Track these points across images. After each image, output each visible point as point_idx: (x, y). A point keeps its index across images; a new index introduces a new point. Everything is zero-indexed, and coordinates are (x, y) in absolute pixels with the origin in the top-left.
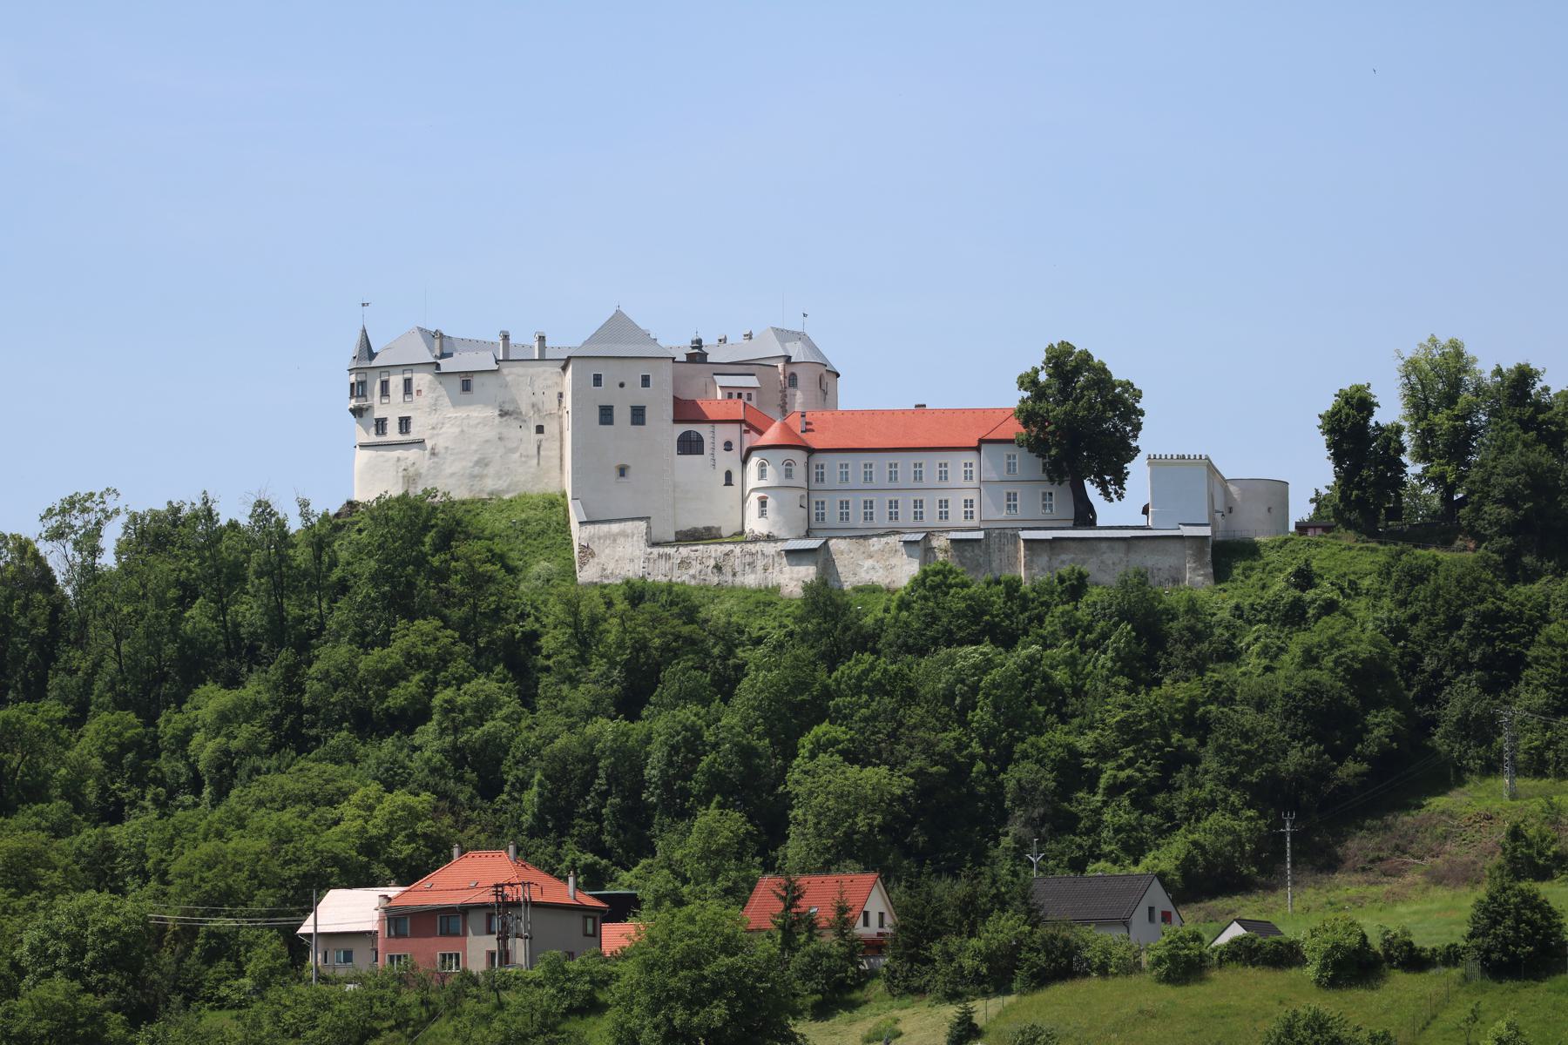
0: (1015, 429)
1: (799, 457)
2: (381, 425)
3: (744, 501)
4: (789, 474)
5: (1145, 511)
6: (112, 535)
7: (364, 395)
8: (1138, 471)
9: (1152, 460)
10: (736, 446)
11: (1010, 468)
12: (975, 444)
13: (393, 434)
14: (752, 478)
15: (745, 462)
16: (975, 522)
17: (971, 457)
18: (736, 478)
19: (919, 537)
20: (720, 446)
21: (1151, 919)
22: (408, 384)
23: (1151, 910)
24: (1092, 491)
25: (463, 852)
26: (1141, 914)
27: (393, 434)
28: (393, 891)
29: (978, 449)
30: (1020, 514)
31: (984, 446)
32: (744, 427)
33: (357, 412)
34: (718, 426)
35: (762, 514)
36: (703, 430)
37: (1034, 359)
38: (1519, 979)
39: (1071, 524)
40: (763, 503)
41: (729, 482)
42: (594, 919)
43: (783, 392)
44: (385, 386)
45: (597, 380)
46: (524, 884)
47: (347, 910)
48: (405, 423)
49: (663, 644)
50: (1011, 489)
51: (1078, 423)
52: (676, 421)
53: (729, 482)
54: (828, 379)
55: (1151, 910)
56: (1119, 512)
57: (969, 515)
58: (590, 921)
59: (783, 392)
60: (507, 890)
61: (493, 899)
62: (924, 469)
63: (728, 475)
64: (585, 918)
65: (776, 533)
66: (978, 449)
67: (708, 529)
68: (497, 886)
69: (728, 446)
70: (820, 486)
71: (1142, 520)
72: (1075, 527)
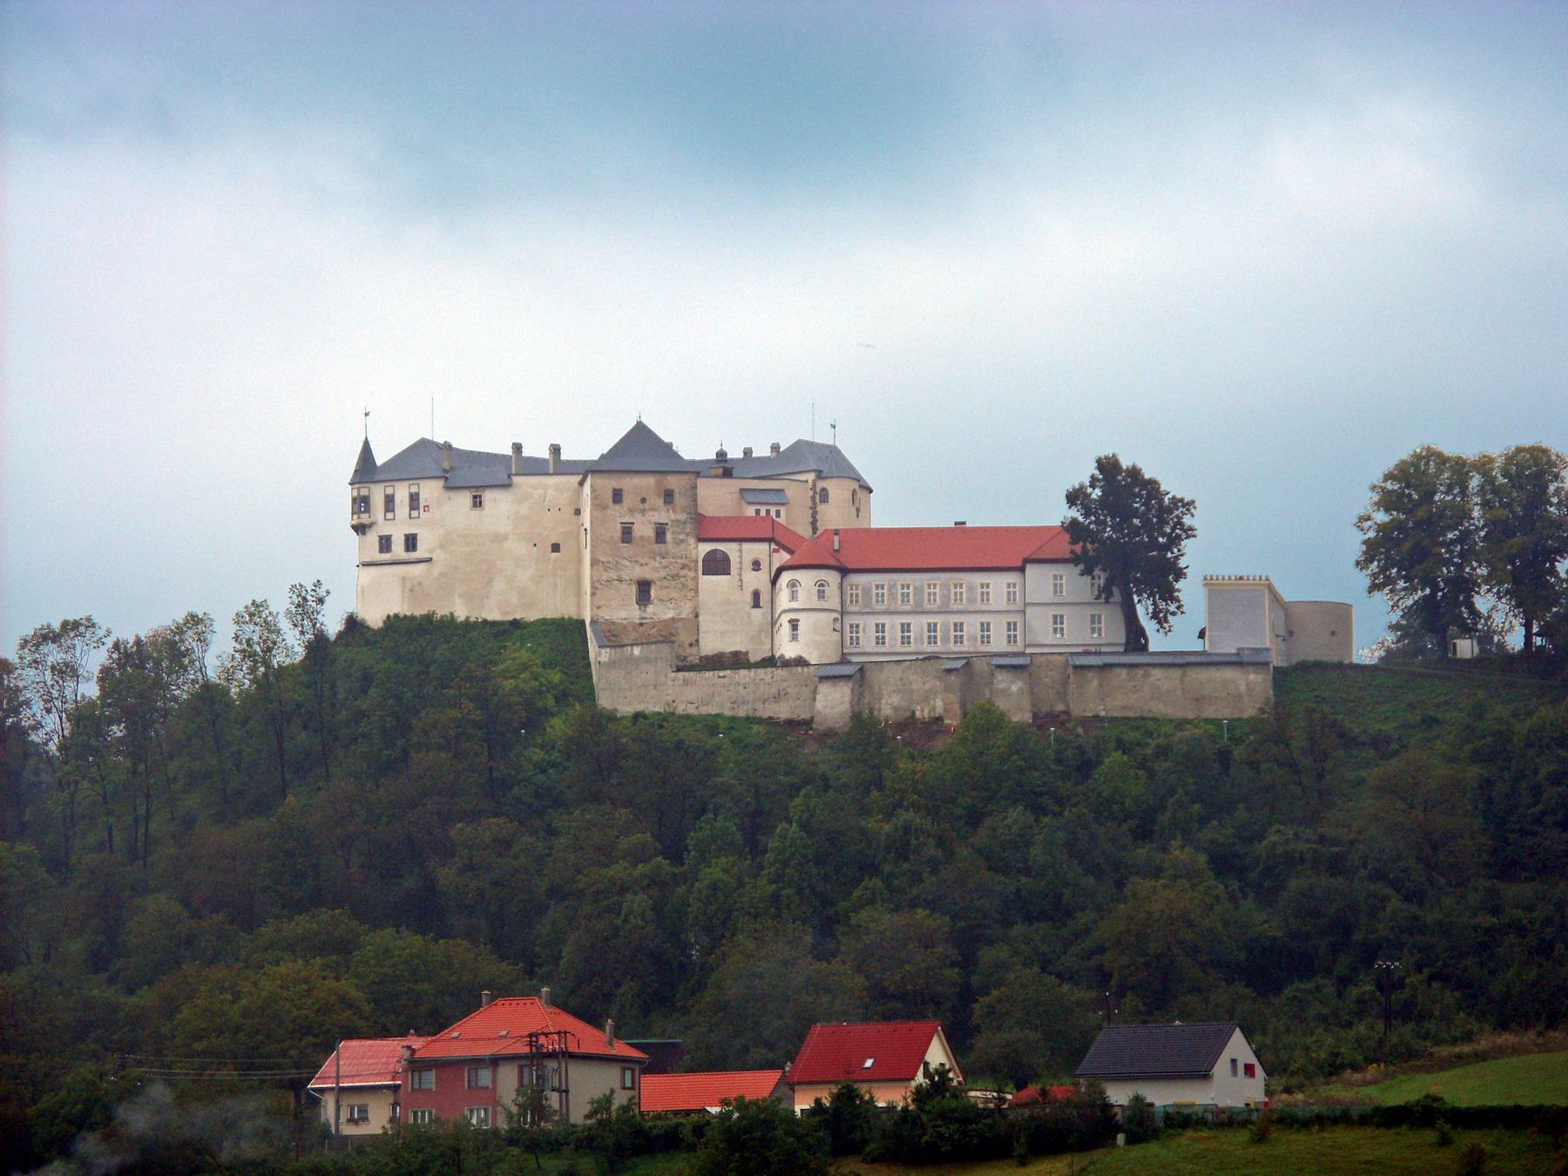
0: (1064, 547)
1: (832, 578)
2: (385, 543)
3: (773, 623)
4: (821, 595)
5: (1202, 635)
6: (94, 660)
7: (367, 510)
8: (1189, 590)
9: (1210, 583)
10: (764, 566)
11: (1057, 589)
12: (1020, 564)
13: (398, 549)
14: (784, 600)
15: (774, 582)
16: (1019, 647)
17: (1012, 577)
18: (765, 598)
19: (959, 664)
20: (747, 565)
21: (1235, 1073)
22: (414, 500)
23: (1234, 1061)
24: (1143, 611)
25: (493, 998)
26: (1221, 1067)
27: (398, 549)
28: (417, 1043)
29: (1022, 569)
30: (1067, 639)
31: (1030, 569)
32: (773, 546)
33: (360, 529)
34: (746, 546)
35: (794, 638)
36: (730, 549)
37: (1083, 472)
38: (1102, 1146)
39: (1122, 649)
40: (794, 625)
41: (756, 604)
42: (633, 1070)
43: (814, 508)
44: (389, 501)
45: (617, 496)
46: (559, 1033)
47: (364, 1062)
48: (411, 542)
49: (669, 775)
50: (1058, 611)
51: (1124, 532)
52: (701, 540)
53: (756, 604)
54: (861, 494)
55: (1234, 1061)
56: (1175, 636)
57: (1011, 639)
58: (628, 1074)
59: (814, 508)
60: (542, 1040)
61: (527, 1050)
62: (991, 590)
63: (756, 595)
64: (624, 1069)
65: (806, 656)
66: (844, 571)
67: (736, 654)
68: (530, 1036)
69: (756, 565)
70: (1012, 618)
71: (1197, 646)
72: (1126, 652)
